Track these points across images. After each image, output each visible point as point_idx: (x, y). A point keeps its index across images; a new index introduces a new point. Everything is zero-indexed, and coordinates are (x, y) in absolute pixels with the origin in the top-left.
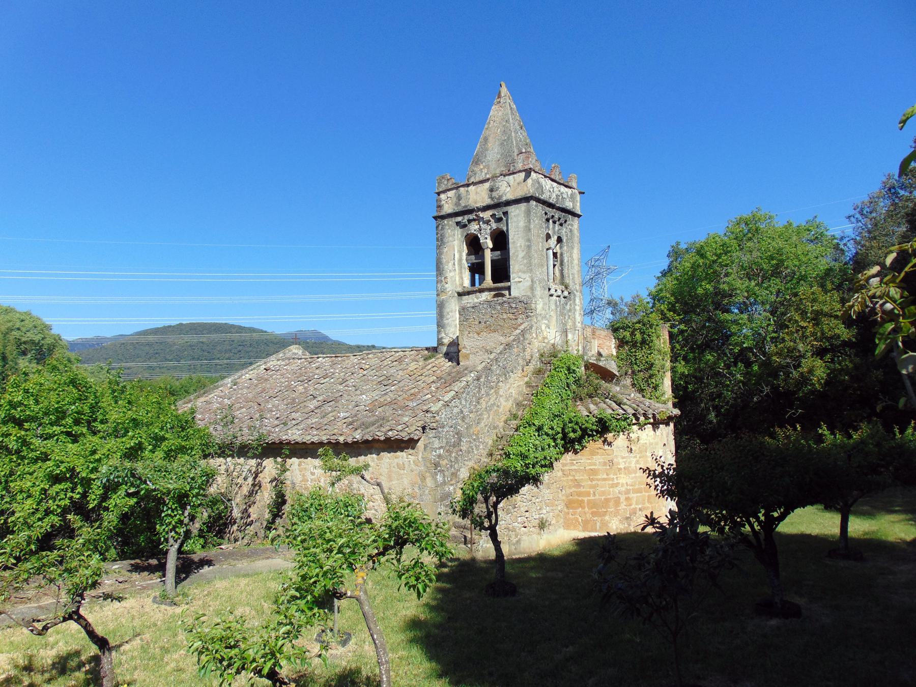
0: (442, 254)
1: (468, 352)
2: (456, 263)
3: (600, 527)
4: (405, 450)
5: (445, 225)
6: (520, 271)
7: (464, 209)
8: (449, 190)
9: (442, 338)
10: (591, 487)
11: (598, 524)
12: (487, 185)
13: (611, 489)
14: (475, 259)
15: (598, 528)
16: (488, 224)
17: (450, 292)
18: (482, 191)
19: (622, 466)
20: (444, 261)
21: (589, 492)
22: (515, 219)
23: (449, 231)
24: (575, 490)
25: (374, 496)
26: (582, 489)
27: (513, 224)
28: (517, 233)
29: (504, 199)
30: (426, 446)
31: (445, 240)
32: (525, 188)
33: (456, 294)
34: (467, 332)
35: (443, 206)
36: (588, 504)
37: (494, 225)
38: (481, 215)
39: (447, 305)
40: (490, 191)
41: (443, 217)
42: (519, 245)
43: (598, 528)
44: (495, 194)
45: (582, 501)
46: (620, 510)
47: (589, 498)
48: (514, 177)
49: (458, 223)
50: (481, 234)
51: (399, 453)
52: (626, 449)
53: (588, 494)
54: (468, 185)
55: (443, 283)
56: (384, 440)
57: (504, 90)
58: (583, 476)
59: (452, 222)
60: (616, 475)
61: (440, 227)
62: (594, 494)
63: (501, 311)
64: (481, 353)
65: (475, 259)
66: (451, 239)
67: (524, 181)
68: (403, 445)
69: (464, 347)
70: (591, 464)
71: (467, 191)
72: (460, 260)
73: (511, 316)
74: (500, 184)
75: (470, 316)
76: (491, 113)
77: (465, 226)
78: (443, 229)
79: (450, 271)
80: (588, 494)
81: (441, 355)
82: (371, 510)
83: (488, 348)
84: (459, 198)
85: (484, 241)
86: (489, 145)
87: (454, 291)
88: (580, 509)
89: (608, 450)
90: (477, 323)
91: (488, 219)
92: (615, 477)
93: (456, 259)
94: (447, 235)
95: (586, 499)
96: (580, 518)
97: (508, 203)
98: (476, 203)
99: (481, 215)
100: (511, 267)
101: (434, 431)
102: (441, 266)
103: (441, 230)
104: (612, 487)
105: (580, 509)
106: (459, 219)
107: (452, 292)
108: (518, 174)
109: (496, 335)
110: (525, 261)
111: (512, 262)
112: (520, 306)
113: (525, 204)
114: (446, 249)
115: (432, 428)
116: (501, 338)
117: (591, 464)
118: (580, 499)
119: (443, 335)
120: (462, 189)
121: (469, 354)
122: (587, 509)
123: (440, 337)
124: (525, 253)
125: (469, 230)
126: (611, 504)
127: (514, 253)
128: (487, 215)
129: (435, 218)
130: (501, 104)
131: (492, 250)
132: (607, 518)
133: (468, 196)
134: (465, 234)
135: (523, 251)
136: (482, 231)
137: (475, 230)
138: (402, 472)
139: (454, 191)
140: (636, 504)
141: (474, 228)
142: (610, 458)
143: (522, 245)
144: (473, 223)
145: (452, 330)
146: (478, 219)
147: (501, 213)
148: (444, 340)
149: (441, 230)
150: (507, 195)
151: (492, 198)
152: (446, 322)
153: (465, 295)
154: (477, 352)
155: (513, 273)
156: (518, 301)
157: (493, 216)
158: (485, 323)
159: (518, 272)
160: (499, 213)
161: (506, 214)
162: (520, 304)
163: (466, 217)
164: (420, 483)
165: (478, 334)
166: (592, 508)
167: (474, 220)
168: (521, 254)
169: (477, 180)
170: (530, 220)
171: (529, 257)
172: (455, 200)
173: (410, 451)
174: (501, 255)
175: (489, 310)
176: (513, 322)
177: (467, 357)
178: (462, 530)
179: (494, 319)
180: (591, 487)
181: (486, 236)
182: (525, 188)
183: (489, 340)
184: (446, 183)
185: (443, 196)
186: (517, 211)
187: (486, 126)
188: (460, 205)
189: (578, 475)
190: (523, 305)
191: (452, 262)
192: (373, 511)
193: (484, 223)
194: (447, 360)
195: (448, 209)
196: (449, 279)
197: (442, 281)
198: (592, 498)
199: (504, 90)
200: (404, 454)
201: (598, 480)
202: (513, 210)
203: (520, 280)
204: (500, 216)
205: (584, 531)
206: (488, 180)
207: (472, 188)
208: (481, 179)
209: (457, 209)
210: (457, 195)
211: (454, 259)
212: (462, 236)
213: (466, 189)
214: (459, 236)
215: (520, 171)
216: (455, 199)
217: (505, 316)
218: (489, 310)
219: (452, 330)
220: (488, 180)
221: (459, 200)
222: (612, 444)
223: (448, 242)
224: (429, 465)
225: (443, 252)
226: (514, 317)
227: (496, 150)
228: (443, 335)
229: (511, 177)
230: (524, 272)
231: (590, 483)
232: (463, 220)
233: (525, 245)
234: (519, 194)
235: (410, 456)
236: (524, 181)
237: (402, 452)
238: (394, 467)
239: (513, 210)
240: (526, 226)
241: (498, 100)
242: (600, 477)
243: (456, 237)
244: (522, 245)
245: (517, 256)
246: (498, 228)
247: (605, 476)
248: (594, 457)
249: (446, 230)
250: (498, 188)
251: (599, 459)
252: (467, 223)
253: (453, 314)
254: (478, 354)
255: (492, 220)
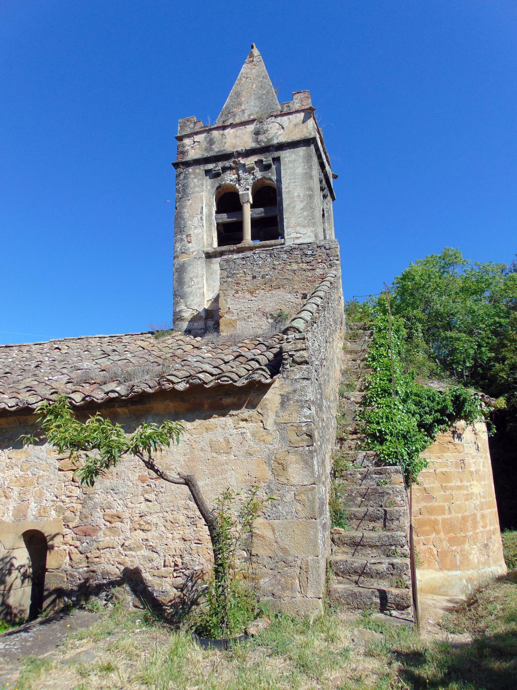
0: (183, 208)
1: (234, 318)
2: (204, 218)
3: (461, 562)
4: (232, 412)
5: (190, 173)
6: (298, 225)
7: (218, 154)
8: (197, 133)
9: (180, 311)
10: (446, 499)
11: (458, 556)
12: (251, 128)
13: (467, 503)
14: (228, 218)
15: (458, 563)
16: (249, 174)
17: (195, 253)
18: (244, 134)
19: (473, 469)
20: (186, 215)
21: (443, 507)
22: (290, 165)
23: (196, 180)
24: (425, 504)
25: (148, 518)
26: (434, 504)
27: (288, 171)
28: (293, 181)
29: (275, 142)
30: (285, 400)
31: (189, 191)
32: (305, 130)
33: (204, 255)
34: (234, 292)
35: (187, 151)
36: (444, 527)
37: (259, 175)
38: (242, 161)
39: (189, 268)
40: (255, 134)
41: (188, 164)
42: (296, 194)
43: (458, 563)
44: (262, 137)
45: (436, 522)
46: (478, 533)
47: (445, 517)
48: (289, 119)
49: (207, 172)
50: (239, 185)
51: (216, 421)
52: (474, 444)
53: (442, 510)
54: (224, 128)
55: (185, 242)
56: (186, 391)
57: (256, 52)
58: (434, 483)
59: (200, 170)
60: (470, 481)
61: (182, 177)
62: (450, 512)
63: (288, 260)
64: (256, 318)
65: (228, 218)
66: (197, 189)
67: (304, 122)
68: (228, 401)
69: (229, 311)
70: (442, 465)
71: (223, 135)
72: (209, 215)
73: (304, 266)
74: (270, 126)
75: (238, 269)
76: (243, 70)
77: (217, 175)
78: (185, 178)
79: (196, 228)
80: (442, 510)
81: (180, 333)
82: (139, 548)
83: (267, 310)
84: (211, 142)
85: (244, 192)
86: (243, 99)
87: (201, 252)
88: (434, 535)
89: (458, 444)
90: (249, 278)
91: (251, 165)
92: (469, 484)
93: (204, 212)
94: (192, 185)
95: (439, 518)
96: (434, 548)
97: (281, 147)
98: (234, 148)
99: (242, 161)
100: (285, 220)
101: (304, 367)
102: (182, 222)
103: (184, 179)
104: (467, 499)
105: (434, 535)
106: (210, 166)
107: (198, 253)
108: (294, 115)
109: (280, 292)
110: (305, 214)
111: (286, 215)
112: (318, 252)
113: (304, 148)
114: (190, 202)
115: (299, 360)
116: (289, 296)
117: (442, 465)
118: (433, 518)
119: (183, 307)
120: (215, 133)
121: (235, 321)
122: (442, 535)
123: (177, 310)
124: (305, 203)
125: (223, 180)
126: (469, 524)
127: (289, 205)
128: (250, 161)
129: (176, 165)
130: (254, 63)
131: (253, 206)
132: (466, 546)
133: (224, 141)
134: (217, 185)
135: (302, 202)
136: (242, 182)
137: (231, 181)
138: (223, 458)
139: (203, 135)
140: (490, 525)
141: (229, 178)
142: (461, 456)
143: (301, 195)
144: (228, 172)
145: (197, 300)
146: (237, 167)
147: (270, 158)
148: (183, 314)
149: (184, 179)
150: (279, 139)
151: (257, 141)
152: (187, 289)
153: (216, 257)
154: (249, 317)
155: (287, 228)
156: (315, 246)
157: (259, 163)
158: (263, 277)
159: (295, 226)
160: (267, 159)
161: (277, 160)
162: (318, 249)
163: (220, 165)
164: (271, 478)
165: (251, 293)
166: (449, 532)
167: (231, 168)
168: (299, 206)
169: (237, 121)
170: (311, 166)
171: (312, 208)
172: (204, 145)
173: (245, 412)
174: (265, 212)
175: (269, 260)
176: (310, 274)
177: (232, 324)
178: (355, 578)
179: (277, 271)
180: (446, 499)
181: (247, 187)
182: (305, 130)
183: (269, 299)
184: (192, 126)
185: (187, 141)
186: (294, 156)
187: (237, 82)
188: (211, 150)
189: (427, 481)
190: (324, 250)
191: (199, 217)
192: (145, 552)
193: (245, 171)
194: (192, 337)
195: (193, 154)
196: (193, 238)
197: (182, 240)
198: (447, 516)
199: (256, 52)
200: (228, 420)
201: (452, 488)
202: (286, 156)
203: (299, 235)
204: (269, 162)
205: (441, 569)
206: (253, 121)
207: (229, 131)
208: (243, 120)
209: (207, 155)
210: (208, 139)
211: (201, 213)
212: (212, 187)
213: (221, 132)
214: (209, 187)
215: (297, 112)
216: (205, 143)
217: (295, 266)
218: (269, 260)
219: (197, 300)
220: (253, 121)
221: (211, 145)
222: (462, 436)
223: (193, 193)
224: (293, 437)
225: (186, 206)
226: (311, 267)
227: (252, 103)
228: (183, 307)
229: (285, 118)
230: (304, 226)
231: (442, 493)
232: (215, 167)
233: (304, 196)
234: (296, 136)
235: (243, 424)
236: (304, 122)
237: (224, 415)
238: (202, 450)
239: (288, 155)
240: (306, 173)
241: (250, 59)
242: (453, 484)
243: (204, 187)
244: (301, 195)
245: (294, 207)
246: (264, 178)
247: (459, 484)
248: (445, 454)
249: (190, 180)
250: (267, 130)
251: (450, 457)
252: (221, 171)
253: (199, 279)
254: (250, 320)
255: (257, 169)
